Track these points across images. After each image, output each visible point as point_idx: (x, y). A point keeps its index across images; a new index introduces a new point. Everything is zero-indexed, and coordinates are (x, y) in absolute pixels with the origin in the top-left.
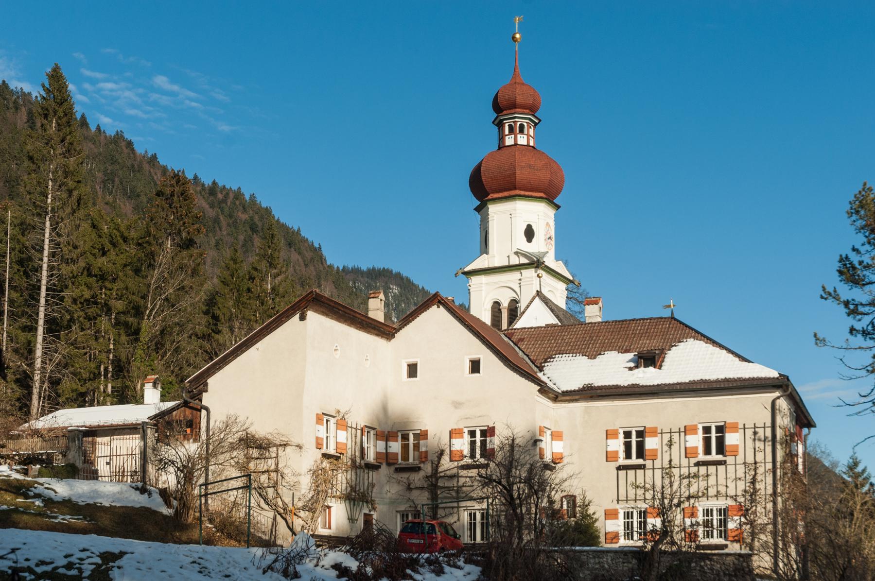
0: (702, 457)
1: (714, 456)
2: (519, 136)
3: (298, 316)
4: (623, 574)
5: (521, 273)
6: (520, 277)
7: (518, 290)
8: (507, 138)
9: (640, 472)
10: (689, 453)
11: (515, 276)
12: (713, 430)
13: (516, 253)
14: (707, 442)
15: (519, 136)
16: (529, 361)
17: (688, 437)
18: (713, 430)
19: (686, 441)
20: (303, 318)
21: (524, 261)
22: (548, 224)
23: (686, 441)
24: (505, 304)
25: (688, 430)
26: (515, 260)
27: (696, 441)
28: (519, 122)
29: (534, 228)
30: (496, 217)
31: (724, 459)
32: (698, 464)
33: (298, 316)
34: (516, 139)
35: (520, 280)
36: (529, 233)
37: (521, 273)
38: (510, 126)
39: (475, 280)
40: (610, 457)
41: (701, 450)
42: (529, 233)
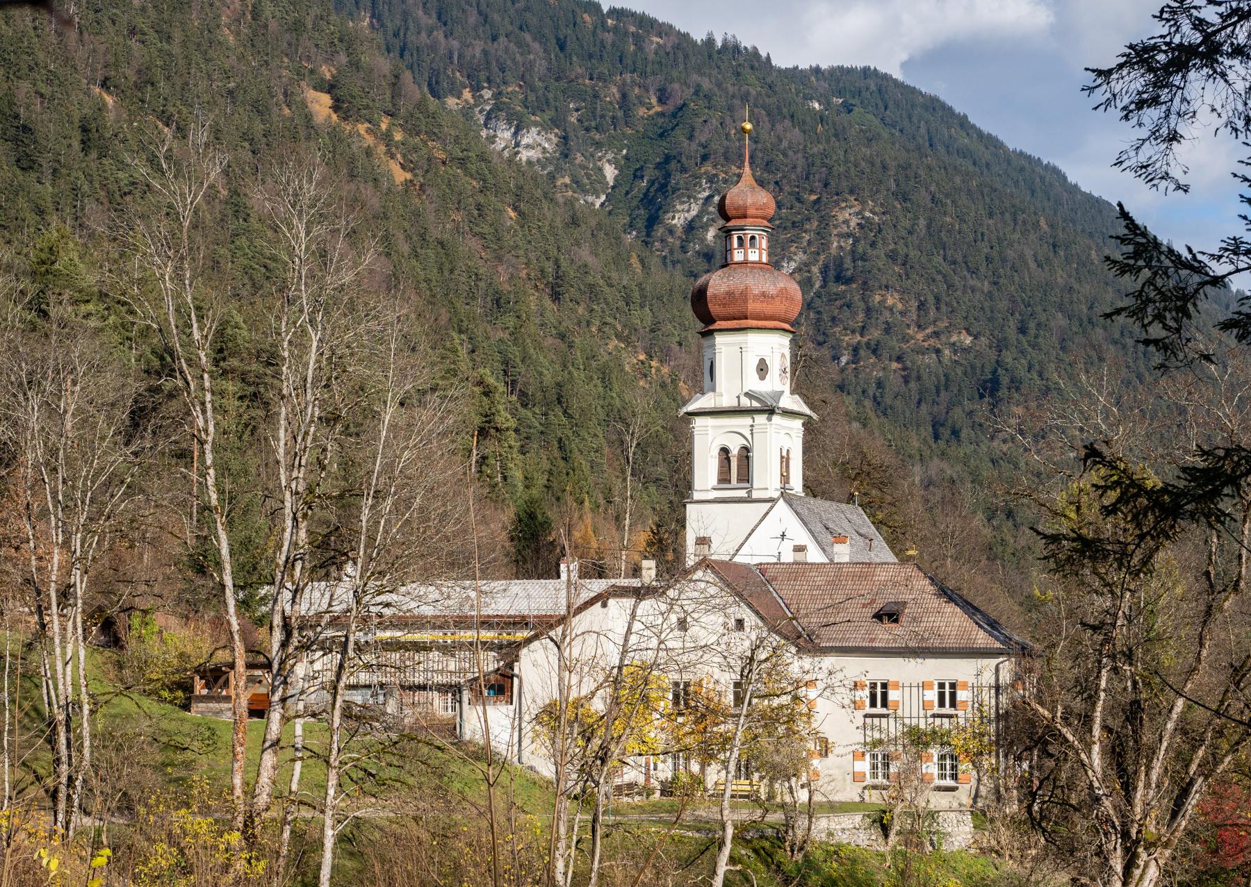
0: (937, 710)
1: (947, 710)
2: (750, 251)
3: (600, 603)
4: (779, 108)
5: (753, 418)
6: (751, 423)
7: (749, 437)
8: (736, 251)
9: (884, 720)
10: (926, 705)
11: (746, 421)
12: (947, 686)
13: (747, 394)
14: (941, 696)
15: (750, 251)
16: (783, 605)
17: (925, 692)
18: (947, 686)
19: (923, 695)
20: (604, 605)
21: (756, 404)
22: (783, 355)
23: (923, 695)
24: (735, 451)
25: (925, 686)
26: (746, 403)
27: (932, 695)
28: (750, 233)
29: (768, 362)
30: (724, 349)
31: (956, 712)
32: (934, 716)
33: (600, 603)
34: (746, 255)
35: (752, 426)
36: (762, 369)
37: (753, 418)
38: (740, 238)
39: (699, 422)
40: (856, 705)
41: (936, 703)
42: (762, 369)
